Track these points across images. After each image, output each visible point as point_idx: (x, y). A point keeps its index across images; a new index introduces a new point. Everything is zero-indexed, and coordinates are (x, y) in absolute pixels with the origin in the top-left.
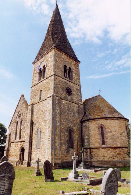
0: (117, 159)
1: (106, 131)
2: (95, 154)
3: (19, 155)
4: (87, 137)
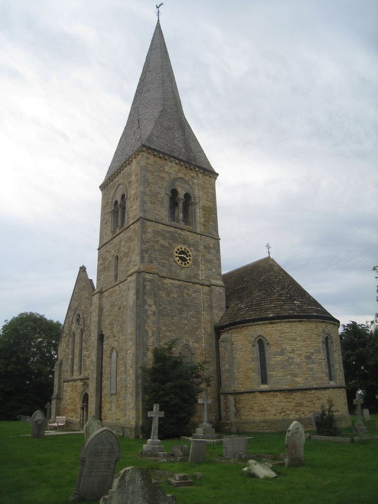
1: (269, 351)
2: (244, 407)
3: (80, 409)
4: (227, 366)
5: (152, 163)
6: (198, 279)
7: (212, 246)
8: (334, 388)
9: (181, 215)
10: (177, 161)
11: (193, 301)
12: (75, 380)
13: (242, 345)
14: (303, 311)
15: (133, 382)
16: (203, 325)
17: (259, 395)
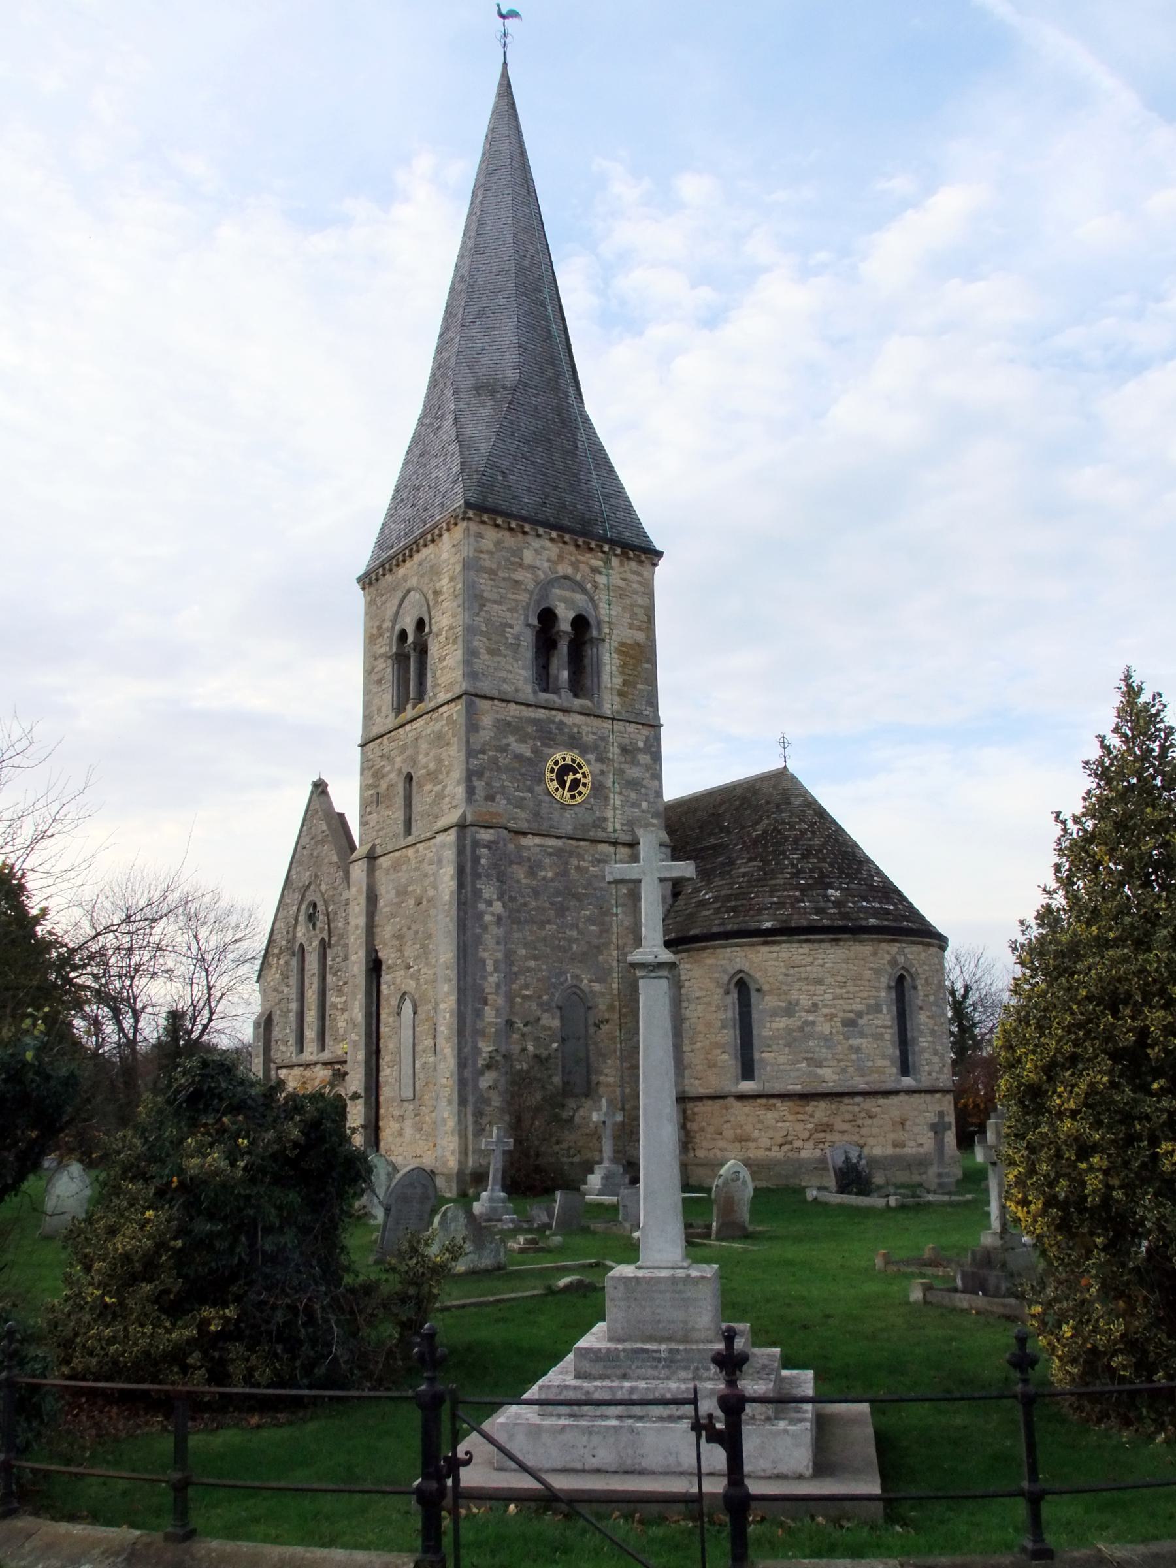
0: (808, 1153)
1: (762, 1005)
5: (491, 547)
6: (604, 830)
7: (641, 744)
8: (910, 1092)
9: (565, 674)
10: (554, 534)
11: (590, 884)
12: (307, 1065)
13: (701, 989)
14: (845, 916)
15: (452, 1075)
16: (615, 940)
17: (737, 1104)
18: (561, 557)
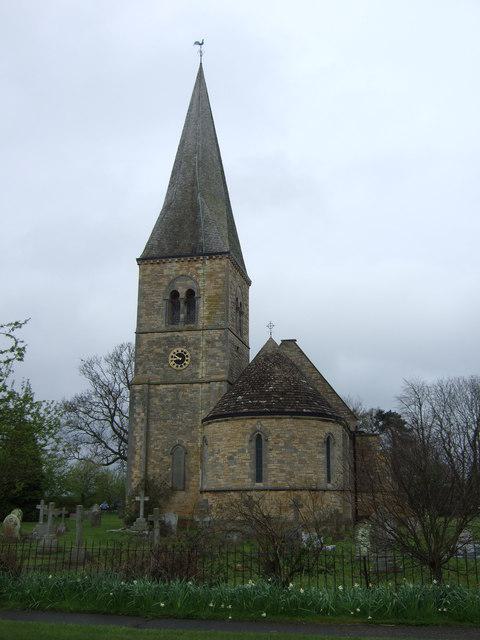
18: (181, 268)
